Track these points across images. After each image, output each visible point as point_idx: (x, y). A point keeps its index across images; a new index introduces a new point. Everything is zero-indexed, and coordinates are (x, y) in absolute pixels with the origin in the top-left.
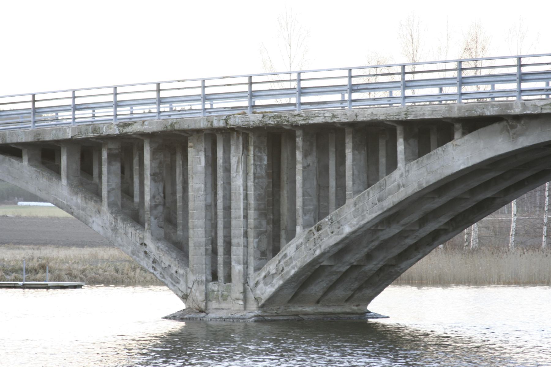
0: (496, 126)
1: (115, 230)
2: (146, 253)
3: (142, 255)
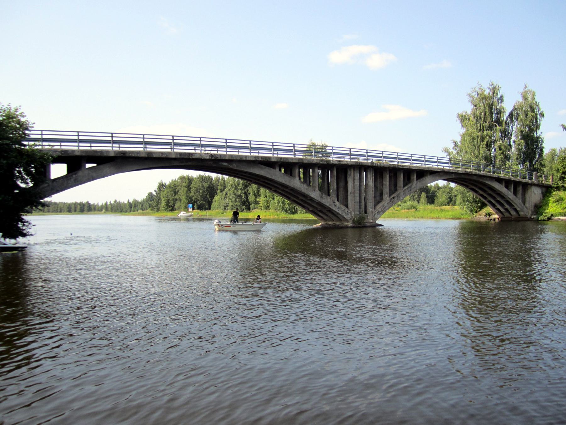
0: (437, 174)
1: (321, 197)
2: (335, 205)
3: (333, 206)
